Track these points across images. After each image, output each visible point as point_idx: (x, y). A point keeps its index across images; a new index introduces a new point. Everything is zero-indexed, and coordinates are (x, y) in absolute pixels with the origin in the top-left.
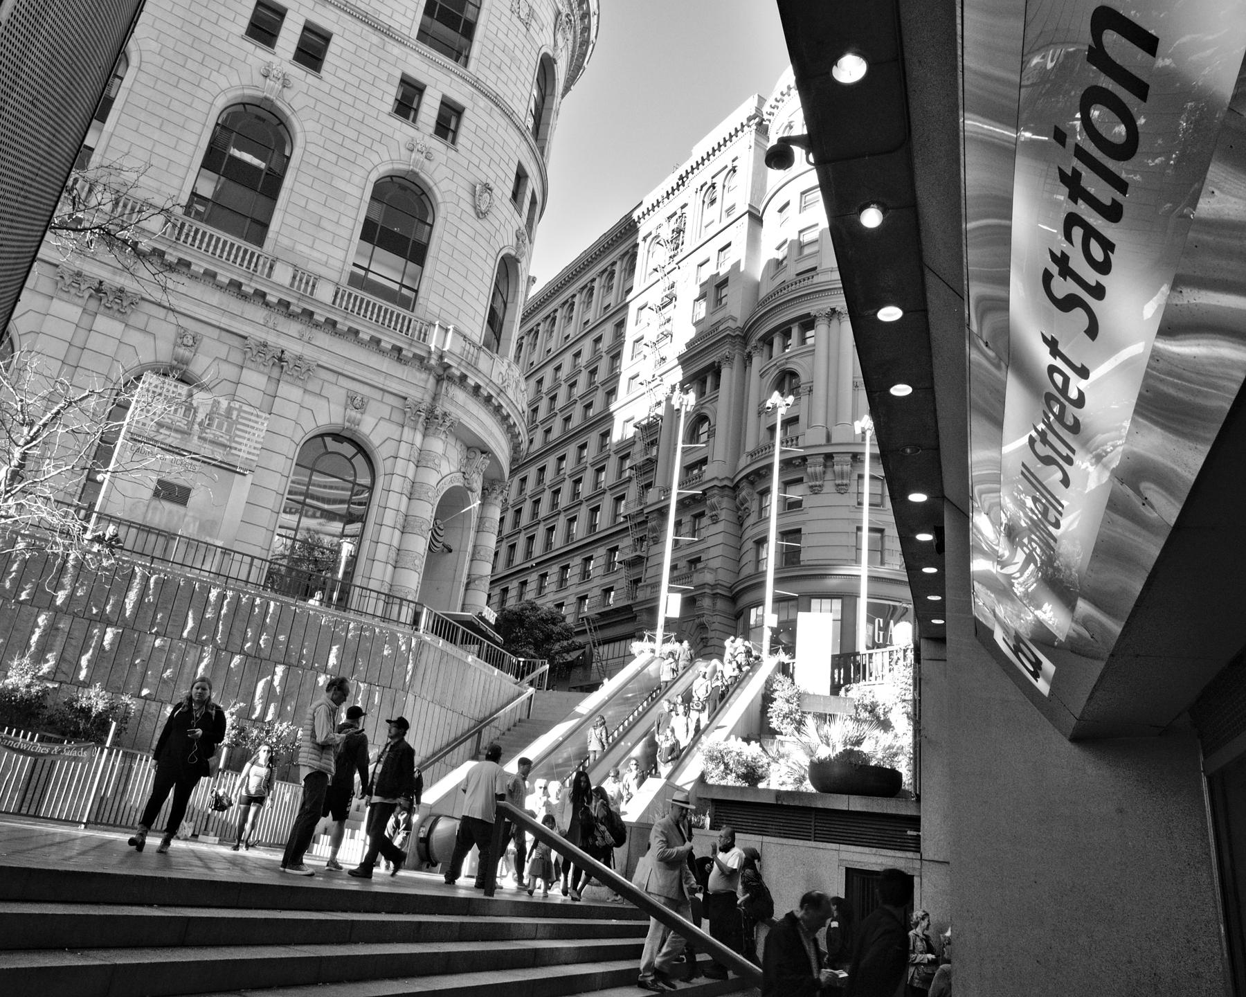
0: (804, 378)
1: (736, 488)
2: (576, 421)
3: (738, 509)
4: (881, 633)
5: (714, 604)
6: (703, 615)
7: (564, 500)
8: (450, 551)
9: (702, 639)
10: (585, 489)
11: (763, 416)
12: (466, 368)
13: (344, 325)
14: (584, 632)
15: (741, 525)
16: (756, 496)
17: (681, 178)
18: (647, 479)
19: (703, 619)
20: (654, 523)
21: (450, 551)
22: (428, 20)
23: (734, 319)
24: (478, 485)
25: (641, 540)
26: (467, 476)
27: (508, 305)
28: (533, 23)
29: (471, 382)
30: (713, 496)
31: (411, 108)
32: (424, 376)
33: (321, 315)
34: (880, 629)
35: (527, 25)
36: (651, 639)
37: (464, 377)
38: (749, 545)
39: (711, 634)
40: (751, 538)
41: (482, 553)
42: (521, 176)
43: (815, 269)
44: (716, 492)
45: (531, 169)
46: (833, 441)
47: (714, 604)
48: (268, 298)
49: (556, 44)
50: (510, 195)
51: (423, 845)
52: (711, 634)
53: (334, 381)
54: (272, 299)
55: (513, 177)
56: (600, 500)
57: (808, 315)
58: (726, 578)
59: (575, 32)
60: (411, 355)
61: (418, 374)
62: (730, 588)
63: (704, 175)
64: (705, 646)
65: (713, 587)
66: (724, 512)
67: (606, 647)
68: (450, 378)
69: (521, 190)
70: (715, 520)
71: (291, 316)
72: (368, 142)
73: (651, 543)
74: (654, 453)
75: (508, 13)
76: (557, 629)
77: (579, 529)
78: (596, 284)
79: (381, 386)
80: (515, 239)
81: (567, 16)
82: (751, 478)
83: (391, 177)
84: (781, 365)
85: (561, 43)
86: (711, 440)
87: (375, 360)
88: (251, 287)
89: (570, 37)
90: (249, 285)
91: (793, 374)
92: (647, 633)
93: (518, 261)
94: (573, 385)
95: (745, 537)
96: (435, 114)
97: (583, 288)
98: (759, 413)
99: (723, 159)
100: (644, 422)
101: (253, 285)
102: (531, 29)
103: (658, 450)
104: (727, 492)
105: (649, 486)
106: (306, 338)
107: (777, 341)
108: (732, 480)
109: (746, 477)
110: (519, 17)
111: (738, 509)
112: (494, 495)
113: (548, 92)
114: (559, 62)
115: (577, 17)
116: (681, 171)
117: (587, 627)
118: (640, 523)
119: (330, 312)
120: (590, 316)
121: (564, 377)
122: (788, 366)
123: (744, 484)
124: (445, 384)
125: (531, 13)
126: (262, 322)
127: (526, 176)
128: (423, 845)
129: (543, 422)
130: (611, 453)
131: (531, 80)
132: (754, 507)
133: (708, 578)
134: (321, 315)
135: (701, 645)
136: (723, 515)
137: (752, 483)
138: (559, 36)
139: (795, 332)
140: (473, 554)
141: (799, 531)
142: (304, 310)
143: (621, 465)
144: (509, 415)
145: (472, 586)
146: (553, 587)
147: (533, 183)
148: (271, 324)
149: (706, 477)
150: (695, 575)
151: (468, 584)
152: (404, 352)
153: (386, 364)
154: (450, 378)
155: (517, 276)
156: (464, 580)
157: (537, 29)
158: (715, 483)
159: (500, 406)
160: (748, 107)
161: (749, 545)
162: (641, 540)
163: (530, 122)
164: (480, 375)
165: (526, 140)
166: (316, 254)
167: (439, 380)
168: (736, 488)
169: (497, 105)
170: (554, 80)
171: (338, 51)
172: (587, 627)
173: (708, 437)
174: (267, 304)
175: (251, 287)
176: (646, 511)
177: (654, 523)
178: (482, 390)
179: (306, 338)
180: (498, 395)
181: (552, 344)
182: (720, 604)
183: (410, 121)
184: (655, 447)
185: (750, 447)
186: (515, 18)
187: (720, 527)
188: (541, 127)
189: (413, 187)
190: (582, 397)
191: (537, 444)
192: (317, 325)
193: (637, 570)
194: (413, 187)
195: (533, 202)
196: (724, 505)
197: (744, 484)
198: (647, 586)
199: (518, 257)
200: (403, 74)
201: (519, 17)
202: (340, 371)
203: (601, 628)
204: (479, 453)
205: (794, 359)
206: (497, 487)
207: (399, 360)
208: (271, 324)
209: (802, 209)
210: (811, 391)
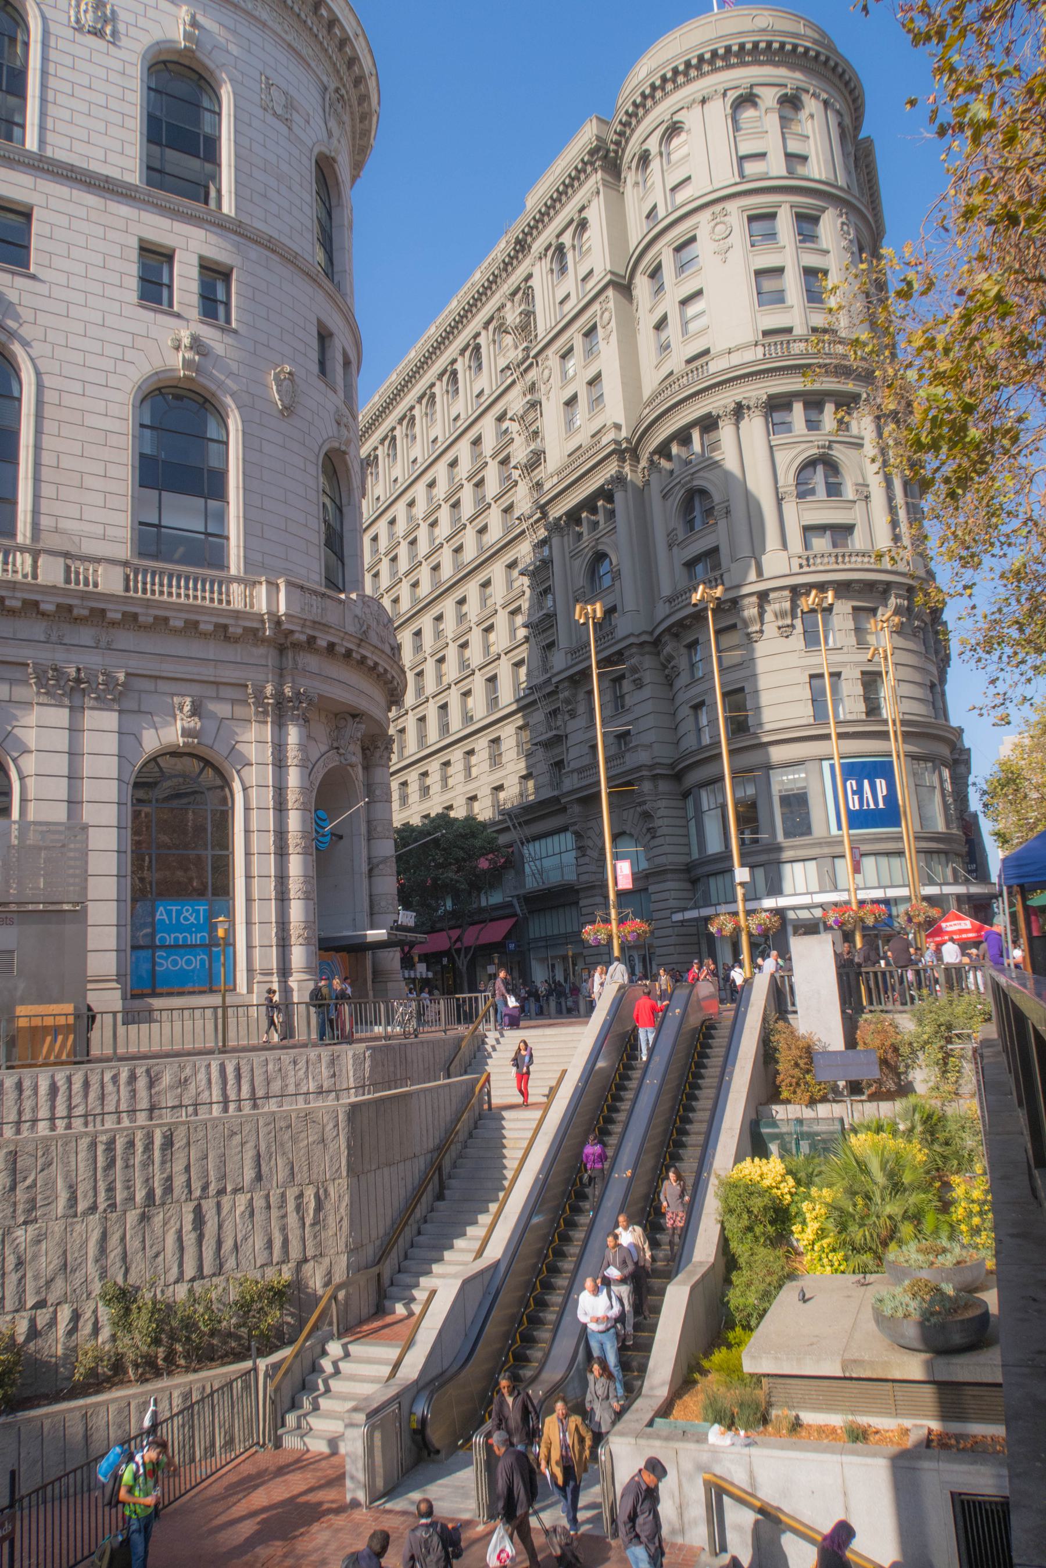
0: (717, 498)
1: (657, 643)
2: (447, 572)
3: (665, 667)
4: (856, 797)
5: (656, 787)
6: (644, 803)
7: (451, 670)
8: (341, 837)
9: (649, 829)
10: (475, 655)
11: (675, 549)
12: (313, 628)
13: (147, 615)
14: (507, 829)
15: (671, 685)
16: (683, 651)
17: (518, 241)
18: (547, 637)
19: (646, 807)
20: (567, 694)
21: (341, 837)
22: (156, 149)
23: (617, 427)
24: (357, 759)
25: (554, 713)
26: (342, 751)
27: (345, 510)
28: (296, 116)
29: (322, 643)
30: (632, 656)
31: (161, 285)
32: (262, 650)
33: (116, 611)
34: (854, 793)
35: (287, 121)
36: (607, 921)
37: (312, 640)
38: (685, 711)
39: (658, 823)
40: (687, 702)
41: (379, 829)
42: (324, 337)
43: (706, 352)
44: (634, 650)
45: (335, 323)
46: (766, 575)
47: (656, 787)
48: (43, 607)
49: (330, 134)
50: (315, 368)
51: (419, 1437)
52: (658, 823)
53: (153, 689)
54: (48, 607)
55: (315, 344)
56: (496, 667)
57: (709, 415)
58: (664, 753)
59: (352, 113)
60: (240, 631)
61: (254, 650)
62: (672, 766)
63: (546, 236)
64: (653, 837)
65: (652, 767)
66: (648, 672)
67: (537, 843)
68: (296, 646)
69: (328, 355)
70: (639, 684)
71: (78, 620)
72: (117, 352)
73: (567, 717)
74: (550, 603)
75: (259, 112)
76: (478, 843)
77: (478, 704)
78: (437, 390)
79: (212, 679)
80: (335, 425)
81: (337, 90)
82: (674, 630)
83: (159, 389)
84: (686, 483)
85: (336, 131)
86: (617, 583)
87: (196, 648)
88: (16, 598)
89: (346, 118)
90: (13, 598)
91: (703, 493)
92: (599, 913)
93: (344, 453)
94: (434, 524)
95: (678, 701)
96: (195, 287)
97: (421, 398)
98: (670, 546)
99: (568, 211)
100: (531, 568)
101: (18, 595)
102: (295, 127)
103: (554, 601)
104: (647, 649)
105: (551, 645)
106: (103, 644)
107: (642, 285)
108: (651, 633)
109: (668, 629)
110: (275, 114)
111: (665, 667)
112: (377, 754)
113: (334, 202)
114: (339, 159)
115: (350, 85)
116: (516, 229)
117: (510, 824)
118: (550, 694)
119: (125, 603)
120: (437, 431)
121: (421, 516)
122: (695, 483)
123: (666, 638)
124: (290, 655)
125: (290, 105)
126: (42, 638)
127: (331, 335)
128: (419, 1437)
129: (407, 574)
130: (498, 607)
131: (308, 198)
132: (682, 663)
133: (643, 757)
134: (116, 611)
135: (649, 836)
136: (648, 677)
137: (676, 636)
138: (333, 124)
139: (696, 435)
140: (369, 832)
141: (742, 690)
142: (92, 610)
143: (512, 623)
144: (376, 664)
145: (376, 872)
146: (460, 777)
147: (341, 340)
148: (54, 638)
149: (620, 633)
150: (627, 755)
151: (370, 871)
152: (231, 629)
153: (212, 650)
154: (296, 646)
155: (348, 470)
156: (365, 868)
157: (302, 123)
158: (632, 640)
159: (364, 658)
160: (588, 134)
161: (685, 711)
162: (554, 713)
163: (320, 256)
164: (332, 631)
165: (320, 286)
166: (87, 527)
167: (282, 650)
168: (657, 643)
169: (273, 251)
170: (338, 184)
171: (46, 230)
172: (510, 824)
173: (613, 579)
174: (44, 614)
175: (16, 598)
176: (554, 680)
177: (567, 694)
178: (337, 648)
179: (103, 644)
180: (359, 646)
181: (397, 471)
182: (663, 786)
183: (165, 307)
184: (550, 596)
185: (666, 591)
186: (270, 118)
187: (647, 692)
188: (335, 254)
189: (192, 395)
190: (448, 540)
191: (405, 605)
192: (113, 624)
193: (557, 751)
194: (192, 395)
195: (347, 363)
196: (646, 665)
197: (666, 638)
198: (572, 772)
199: (343, 448)
200: (141, 240)
201: (275, 114)
202: (157, 674)
203: (527, 822)
204: (350, 719)
205: (701, 474)
206: (379, 744)
207: (227, 638)
208: (54, 638)
209: (681, 268)
210: (728, 512)
